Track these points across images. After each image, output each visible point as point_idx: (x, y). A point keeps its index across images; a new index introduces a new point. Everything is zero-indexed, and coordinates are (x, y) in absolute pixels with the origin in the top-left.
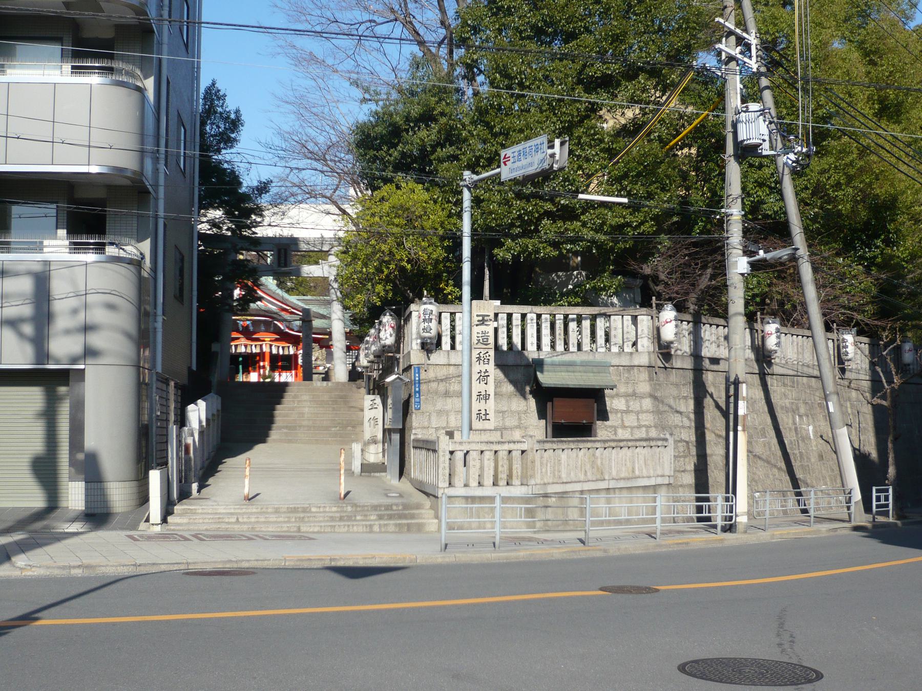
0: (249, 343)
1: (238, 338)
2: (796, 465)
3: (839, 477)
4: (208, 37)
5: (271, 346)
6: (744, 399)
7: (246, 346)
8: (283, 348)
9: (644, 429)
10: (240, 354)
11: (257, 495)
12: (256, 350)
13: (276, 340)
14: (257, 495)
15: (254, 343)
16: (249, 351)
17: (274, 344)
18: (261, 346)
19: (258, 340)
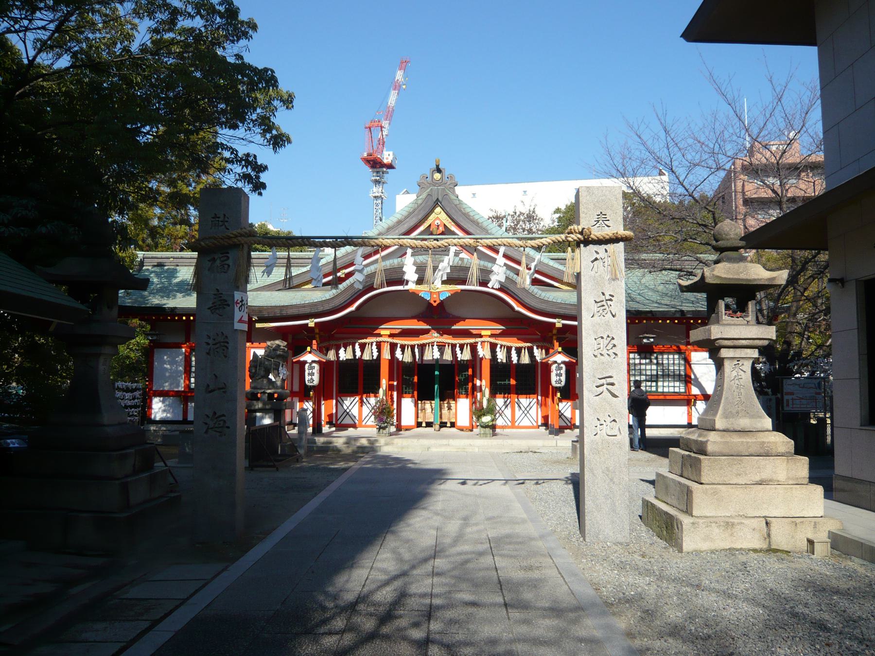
0: (448, 339)
1: (426, 332)
2: (733, 453)
3: (715, 486)
4: (857, 376)
5: (493, 347)
6: (274, 254)
7: (441, 347)
8: (519, 350)
9: (695, 422)
10: (436, 364)
11: (643, 480)
12: (465, 356)
13: (503, 334)
14: (643, 480)
15: (458, 341)
16: (448, 356)
17: (499, 342)
18: (473, 348)
19: (466, 333)
